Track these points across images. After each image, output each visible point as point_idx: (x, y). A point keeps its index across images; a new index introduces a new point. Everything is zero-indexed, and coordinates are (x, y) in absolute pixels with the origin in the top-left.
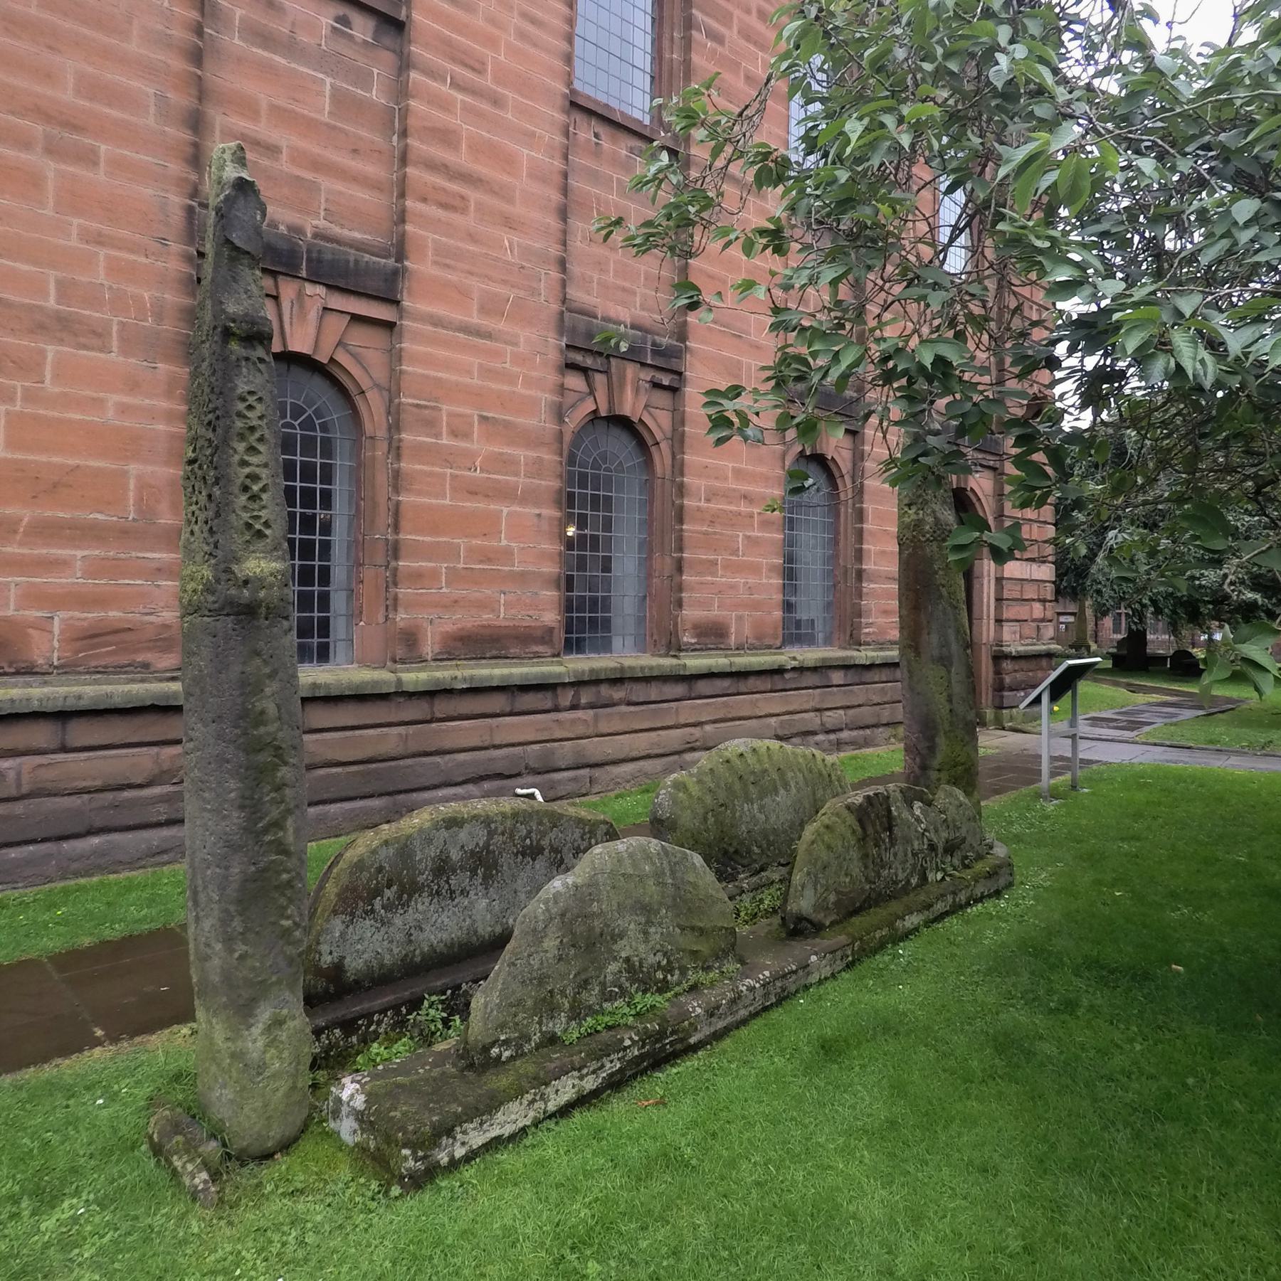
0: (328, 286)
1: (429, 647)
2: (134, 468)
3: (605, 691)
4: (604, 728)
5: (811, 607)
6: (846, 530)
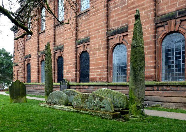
0: (120, 33)
1: (98, 80)
2: (103, 61)
3: (164, 87)
4: (164, 95)
5: (29, 60)
6: (134, 8)
